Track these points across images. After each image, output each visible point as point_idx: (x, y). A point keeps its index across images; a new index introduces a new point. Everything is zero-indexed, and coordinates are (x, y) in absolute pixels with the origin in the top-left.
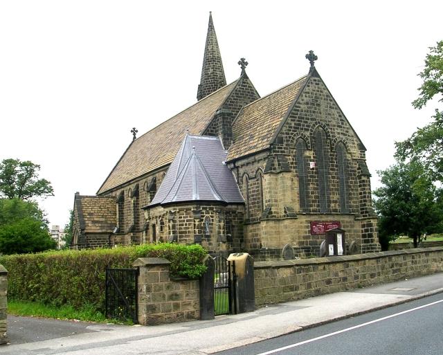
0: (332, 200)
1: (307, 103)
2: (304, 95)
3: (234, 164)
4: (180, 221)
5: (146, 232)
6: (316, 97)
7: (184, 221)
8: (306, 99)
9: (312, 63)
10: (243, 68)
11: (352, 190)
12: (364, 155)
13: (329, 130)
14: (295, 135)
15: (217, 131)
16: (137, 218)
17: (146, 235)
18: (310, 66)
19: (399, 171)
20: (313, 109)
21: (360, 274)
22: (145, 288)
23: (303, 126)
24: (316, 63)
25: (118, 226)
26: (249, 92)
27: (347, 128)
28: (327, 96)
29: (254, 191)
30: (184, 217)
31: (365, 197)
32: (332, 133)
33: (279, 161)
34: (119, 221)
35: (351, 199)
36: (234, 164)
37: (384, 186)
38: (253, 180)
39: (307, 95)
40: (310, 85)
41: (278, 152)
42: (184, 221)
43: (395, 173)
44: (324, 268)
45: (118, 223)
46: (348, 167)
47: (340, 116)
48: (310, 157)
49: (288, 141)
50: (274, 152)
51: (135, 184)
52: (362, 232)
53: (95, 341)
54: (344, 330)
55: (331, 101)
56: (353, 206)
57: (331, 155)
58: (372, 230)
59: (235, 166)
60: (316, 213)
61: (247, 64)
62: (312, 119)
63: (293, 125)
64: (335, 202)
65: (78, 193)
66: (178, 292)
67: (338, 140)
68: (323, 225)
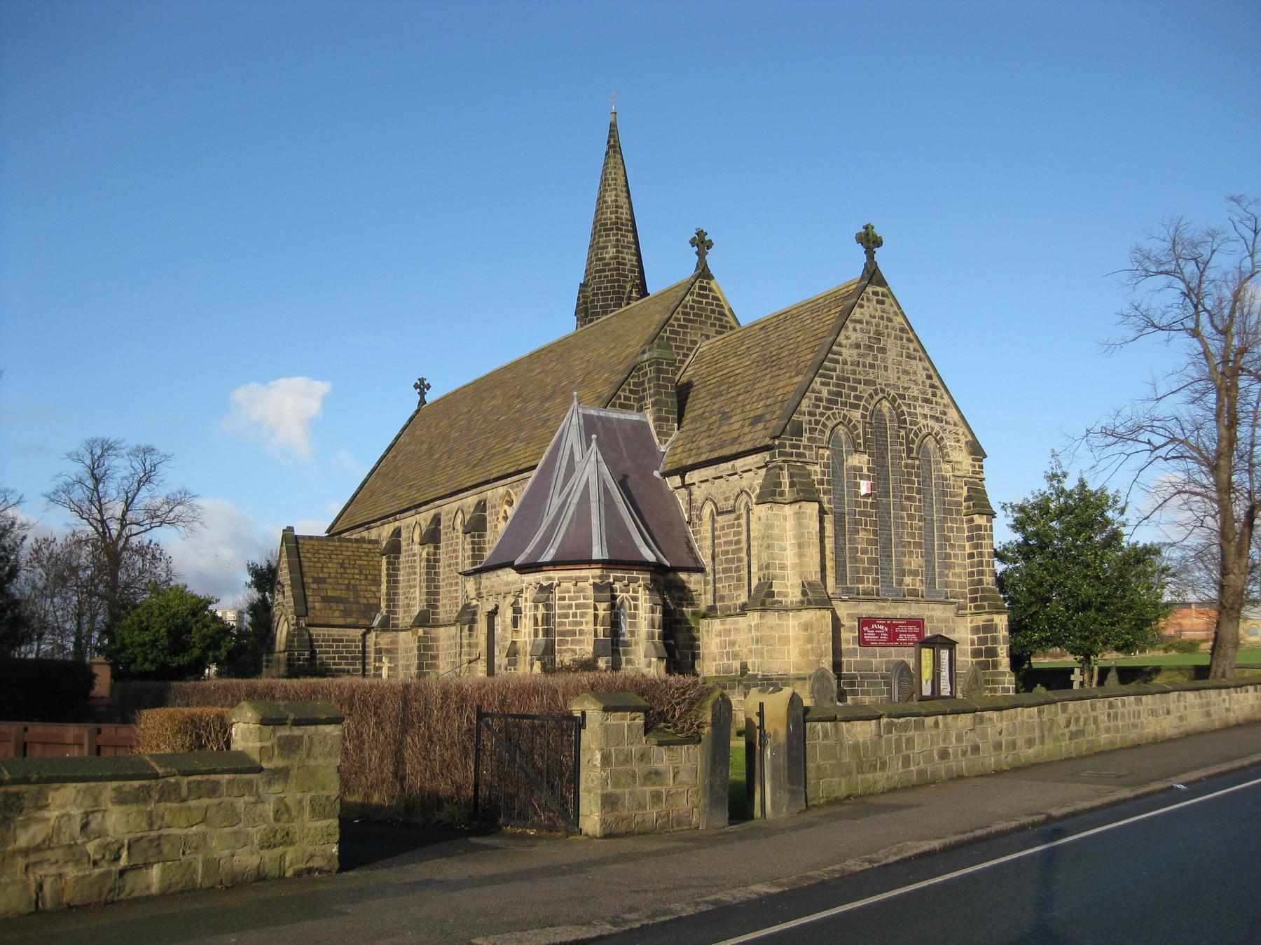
0: (907, 567)
1: (858, 346)
2: (851, 326)
3: (683, 478)
4: (561, 607)
5: (471, 629)
6: (878, 333)
7: (570, 607)
8: (854, 337)
9: (870, 254)
10: (701, 255)
11: (953, 546)
12: (981, 467)
13: (905, 409)
14: (828, 418)
15: (643, 399)
16: (432, 593)
17: (470, 636)
18: (864, 259)
19: (1052, 506)
20: (869, 360)
21: (1004, 739)
22: (598, 756)
23: (848, 396)
24: (879, 254)
25: (384, 610)
26: (713, 311)
27: (945, 405)
28: (902, 330)
29: (728, 543)
30: (571, 599)
31: (980, 564)
32: (910, 414)
33: (791, 476)
34: (388, 600)
35: (948, 566)
36: (683, 478)
37: (1018, 537)
38: (727, 517)
39: (858, 326)
40: (865, 303)
41: (791, 455)
42: (570, 607)
43: (1042, 507)
44: (936, 724)
45: (383, 604)
46: (944, 494)
47: (929, 377)
48: (861, 469)
49: (812, 430)
50: (781, 454)
51: (433, 512)
52: (972, 643)
53: (489, 869)
54: (793, 924)
55: (909, 340)
56: (954, 585)
57: (907, 466)
58: (995, 640)
59: (683, 482)
60: (870, 596)
61: (709, 245)
62: (867, 383)
63: (825, 394)
64: (914, 573)
65: (291, 529)
66: (660, 766)
67: (924, 432)
68: (885, 625)
